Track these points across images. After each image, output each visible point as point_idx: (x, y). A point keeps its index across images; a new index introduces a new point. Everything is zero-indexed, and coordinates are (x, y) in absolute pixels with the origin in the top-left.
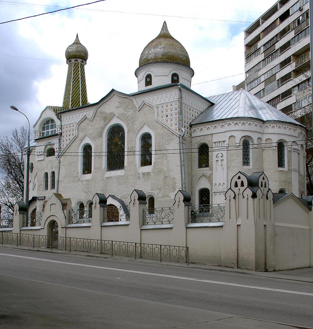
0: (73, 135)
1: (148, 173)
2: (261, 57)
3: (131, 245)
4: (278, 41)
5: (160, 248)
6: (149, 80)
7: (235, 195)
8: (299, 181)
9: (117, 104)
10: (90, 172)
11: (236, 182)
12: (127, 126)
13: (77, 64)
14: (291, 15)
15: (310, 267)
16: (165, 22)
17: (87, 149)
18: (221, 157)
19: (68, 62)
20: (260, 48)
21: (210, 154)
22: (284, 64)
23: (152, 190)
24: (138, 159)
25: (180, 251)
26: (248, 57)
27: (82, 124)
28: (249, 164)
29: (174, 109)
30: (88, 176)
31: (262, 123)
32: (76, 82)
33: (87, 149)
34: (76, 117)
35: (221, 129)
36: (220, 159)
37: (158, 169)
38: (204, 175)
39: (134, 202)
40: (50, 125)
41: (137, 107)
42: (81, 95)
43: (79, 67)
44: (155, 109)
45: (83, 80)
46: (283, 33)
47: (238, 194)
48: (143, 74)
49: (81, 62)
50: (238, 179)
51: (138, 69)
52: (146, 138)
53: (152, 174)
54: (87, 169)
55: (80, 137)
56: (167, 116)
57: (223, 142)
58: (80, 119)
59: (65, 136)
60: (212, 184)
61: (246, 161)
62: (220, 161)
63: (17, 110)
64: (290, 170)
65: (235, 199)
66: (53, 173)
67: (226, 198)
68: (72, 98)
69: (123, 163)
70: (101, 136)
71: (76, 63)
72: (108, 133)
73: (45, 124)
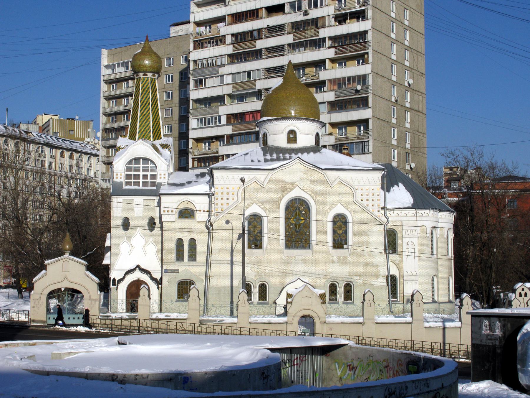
1: (345, 258)
13: (139, 79)
40: (141, 165)
53: (350, 259)
70: (279, 208)
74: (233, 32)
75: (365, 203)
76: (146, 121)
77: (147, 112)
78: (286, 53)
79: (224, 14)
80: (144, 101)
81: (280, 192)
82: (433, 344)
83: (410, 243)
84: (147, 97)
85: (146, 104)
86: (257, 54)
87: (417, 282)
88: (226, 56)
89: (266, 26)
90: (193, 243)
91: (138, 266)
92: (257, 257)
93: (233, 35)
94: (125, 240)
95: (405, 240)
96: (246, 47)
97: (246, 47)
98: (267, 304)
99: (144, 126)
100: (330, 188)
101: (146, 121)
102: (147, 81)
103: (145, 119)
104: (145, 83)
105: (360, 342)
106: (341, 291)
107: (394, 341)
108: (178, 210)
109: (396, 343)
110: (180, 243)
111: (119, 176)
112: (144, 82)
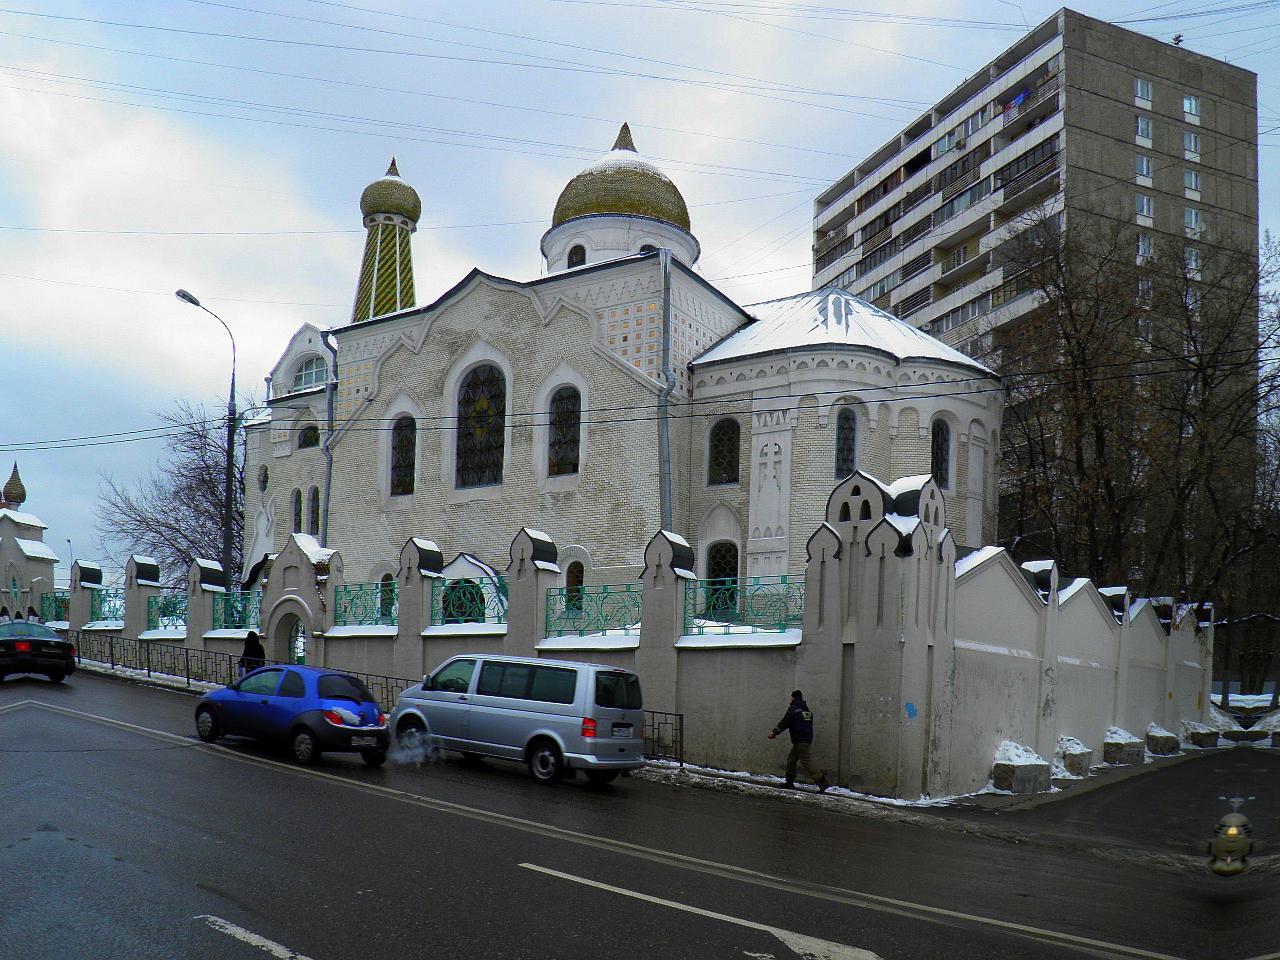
0: (366, 389)
1: (569, 496)
2: (855, 255)
4: (899, 218)
6: (577, 255)
7: (840, 544)
8: (983, 528)
9: (487, 309)
11: (846, 506)
12: (514, 365)
13: (391, 227)
14: (936, 159)
16: (625, 127)
17: (404, 429)
18: (776, 453)
19: (368, 219)
20: (853, 235)
21: (743, 446)
22: (910, 270)
24: (540, 451)
25: (656, 726)
26: (822, 259)
27: (392, 361)
29: (645, 321)
30: (404, 501)
31: (891, 364)
32: (386, 271)
33: (404, 429)
34: (381, 339)
35: (778, 377)
36: (772, 458)
38: (724, 505)
39: (521, 566)
41: (542, 314)
43: (395, 236)
44: (592, 318)
45: (404, 269)
46: (912, 200)
47: (852, 543)
48: (563, 245)
49: (402, 223)
50: (853, 494)
51: (549, 232)
52: (566, 407)
54: (402, 482)
55: (383, 396)
56: (625, 339)
57: (781, 413)
58: (384, 350)
59: (345, 392)
60: (745, 531)
61: (845, 467)
62: (770, 465)
63: (195, 302)
64: (962, 497)
65: (840, 559)
66: (315, 492)
67: (810, 558)
68: (375, 308)
69: (499, 465)
70: (442, 394)
71: (387, 225)
72: (462, 386)
73: (300, 370)
81: (445, 358)
95: (757, 443)
96: (880, 241)
97: (880, 241)
105: (145, 645)
108: (501, 483)
112: (387, 232)
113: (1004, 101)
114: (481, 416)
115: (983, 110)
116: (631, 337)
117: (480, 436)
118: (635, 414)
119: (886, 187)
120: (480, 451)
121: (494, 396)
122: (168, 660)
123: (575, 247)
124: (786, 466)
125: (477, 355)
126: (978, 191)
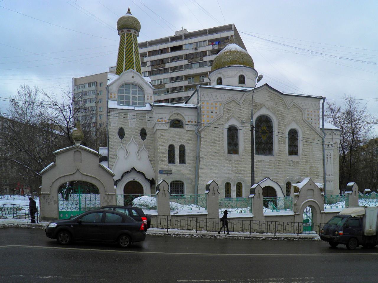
1: (298, 162)
3: (255, 223)
5: (319, 226)
10: (236, 152)
13: (124, 34)
15: (53, 183)
23: (301, 176)
28: (297, 154)
37: (306, 159)
42: (125, 47)
52: (293, 135)
53: (300, 163)
74: (151, 60)
75: (310, 121)
76: (130, 62)
77: (131, 56)
78: (183, 69)
79: (146, 51)
80: (128, 49)
82: (285, 224)
83: (329, 154)
84: (130, 46)
85: (130, 51)
86: (166, 71)
87: (333, 181)
88: (147, 72)
89: (171, 56)
90: (182, 150)
91: (133, 169)
92: (236, 161)
93: (151, 61)
94: (122, 146)
96: (158, 68)
98: (185, 198)
99: (129, 66)
100: (287, 109)
101: (130, 62)
102: (130, 35)
103: (130, 61)
104: (129, 37)
106: (234, 189)
107: (282, 223)
109: (268, 225)
110: (171, 148)
111: (113, 95)
113: (212, 42)
114: (264, 133)
115: (204, 41)
116: (313, 119)
117: (264, 138)
118: (316, 142)
119: (162, 51)
120: (264, 143)
121: (268, 126)
122: (238, 226)
123: (241, 75)
124: (332, 159)
125: (263, 112)
126: (202, 64)
